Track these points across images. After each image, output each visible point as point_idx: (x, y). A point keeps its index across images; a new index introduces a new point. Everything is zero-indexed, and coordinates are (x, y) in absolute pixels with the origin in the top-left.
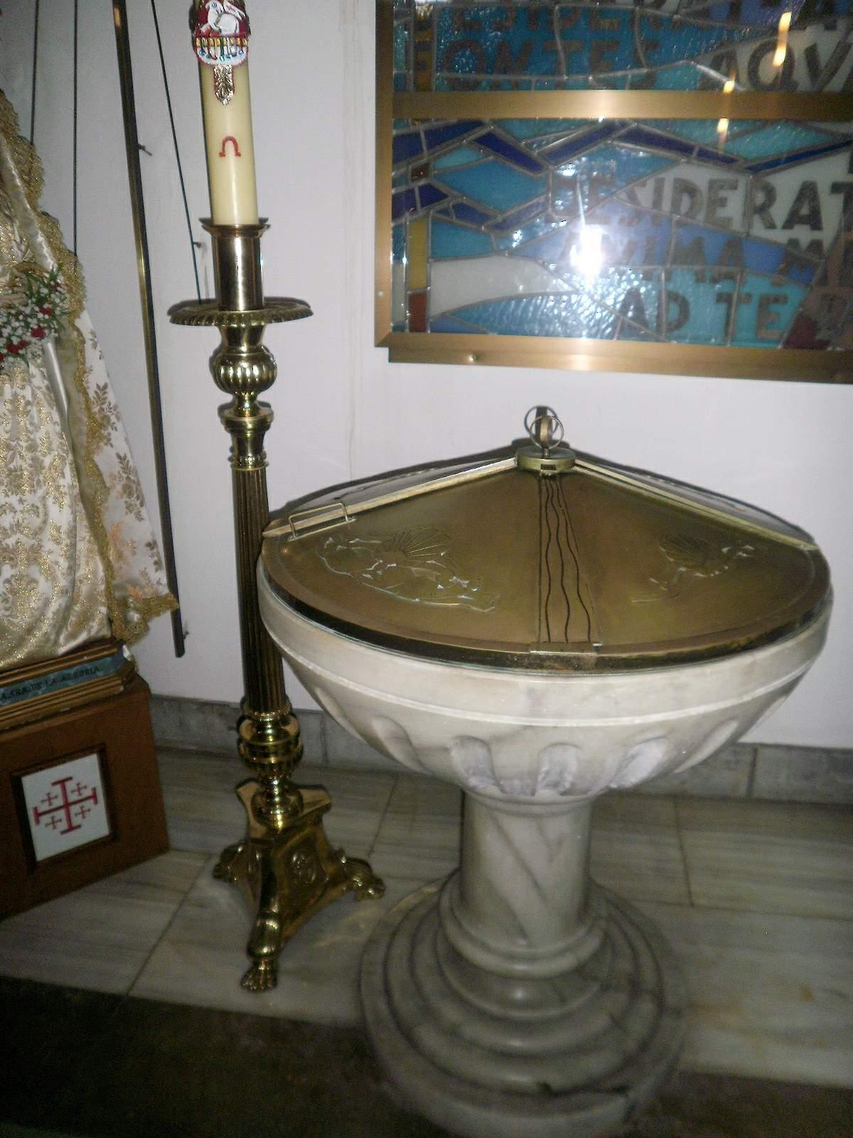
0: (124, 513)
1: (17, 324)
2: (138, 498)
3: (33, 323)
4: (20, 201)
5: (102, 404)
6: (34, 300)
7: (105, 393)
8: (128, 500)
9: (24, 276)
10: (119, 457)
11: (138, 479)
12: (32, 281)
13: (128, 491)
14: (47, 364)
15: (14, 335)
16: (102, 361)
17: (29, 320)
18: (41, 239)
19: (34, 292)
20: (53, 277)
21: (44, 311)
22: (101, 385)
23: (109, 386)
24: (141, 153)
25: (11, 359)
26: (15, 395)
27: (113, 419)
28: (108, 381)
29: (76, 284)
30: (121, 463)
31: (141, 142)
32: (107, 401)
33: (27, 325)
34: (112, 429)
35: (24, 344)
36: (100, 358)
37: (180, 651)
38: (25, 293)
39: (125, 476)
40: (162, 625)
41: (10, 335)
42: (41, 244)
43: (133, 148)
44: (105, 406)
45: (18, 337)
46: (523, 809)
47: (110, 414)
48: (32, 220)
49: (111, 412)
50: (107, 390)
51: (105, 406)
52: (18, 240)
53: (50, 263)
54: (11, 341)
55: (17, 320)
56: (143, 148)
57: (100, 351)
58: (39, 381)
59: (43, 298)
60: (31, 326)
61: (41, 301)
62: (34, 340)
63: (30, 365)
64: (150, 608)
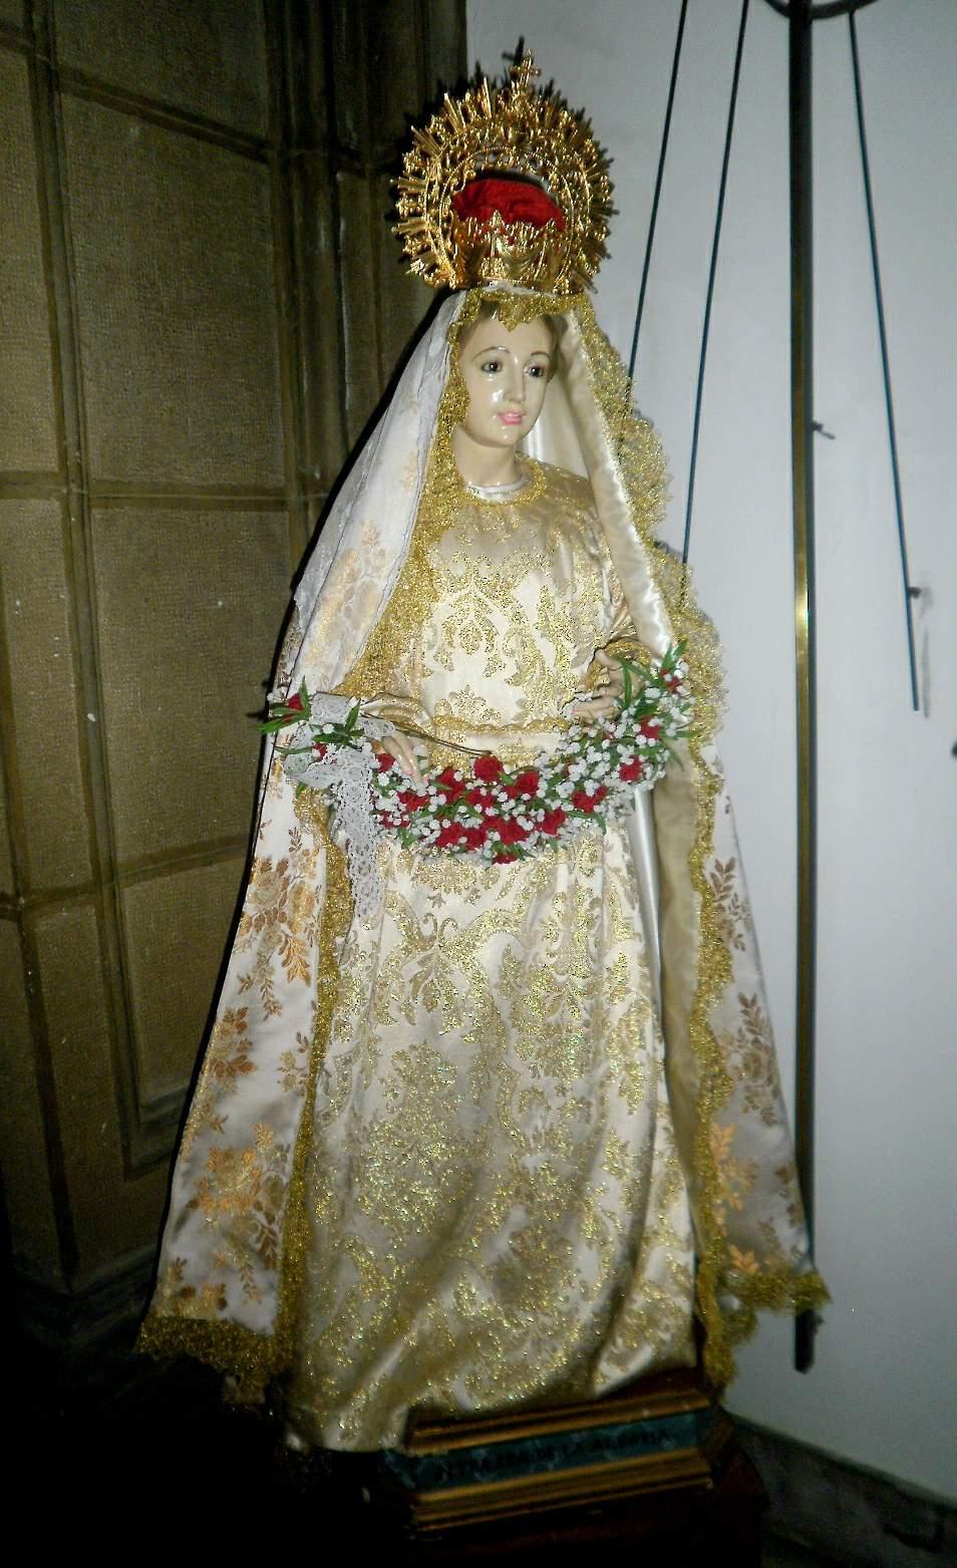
0: (740, 1109)
1: (598, 757)
2: (770, 1080)
3: (626, 753)
4: (624, 529)
5: (722, 898)
6: (632, 710)
7: (729, 878)
8: (751, 1083)
9: (618, 665)
10: (743, 1000)
11: (773, 1043)
12: (632, 675)
13: (753, 1066)
14: (629, 827)
15: (589, 778)
16: (728, 816)
17: (620, 748)
18: (651, 597)
19: (634, 694)
20: (668, 668)
21: (648, 732)
22: (724, 863)
23: (737, 864)
24: (817, 438)
25: (577, 821)
26: (574, 888)
27: (739, 927)
28: (736, 856)
29: (708, 684)
30: (745, 1012)
31: (817, 417)
32: (732, 892)
33: (616, 757)
34: (736, 946)
35: (602, 792)
36: (727, 812)
37: (803, 1357)
38: (617, 698)
39: (750, 1037)
40: (776, 1327)
41: (583, 778)
42: (650, 606)
43: (804, 428)
44: (726, 903)
45: (595, 780)
46: (54, 229)
47: (734, 918)
48: (637, 561)
49: (736, 914)
50: (733, 873)
51: (726, 903)
52: (607, 596)
53: (663, 641)
54: (583, 791)
55: (599, 749)
56: (818, 427)
57: (728, 798)
58: (617, 858)
59: (647, 706)
60: (622, 760)
61: (644, 712)
62: (623, 786)
63: (608, 829)
64: (760, 1294)
